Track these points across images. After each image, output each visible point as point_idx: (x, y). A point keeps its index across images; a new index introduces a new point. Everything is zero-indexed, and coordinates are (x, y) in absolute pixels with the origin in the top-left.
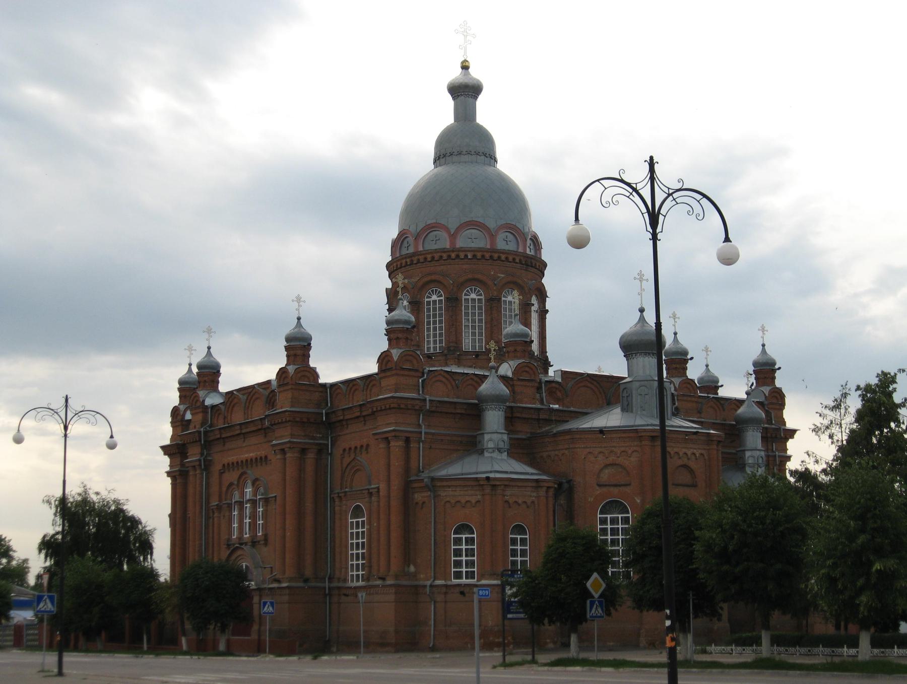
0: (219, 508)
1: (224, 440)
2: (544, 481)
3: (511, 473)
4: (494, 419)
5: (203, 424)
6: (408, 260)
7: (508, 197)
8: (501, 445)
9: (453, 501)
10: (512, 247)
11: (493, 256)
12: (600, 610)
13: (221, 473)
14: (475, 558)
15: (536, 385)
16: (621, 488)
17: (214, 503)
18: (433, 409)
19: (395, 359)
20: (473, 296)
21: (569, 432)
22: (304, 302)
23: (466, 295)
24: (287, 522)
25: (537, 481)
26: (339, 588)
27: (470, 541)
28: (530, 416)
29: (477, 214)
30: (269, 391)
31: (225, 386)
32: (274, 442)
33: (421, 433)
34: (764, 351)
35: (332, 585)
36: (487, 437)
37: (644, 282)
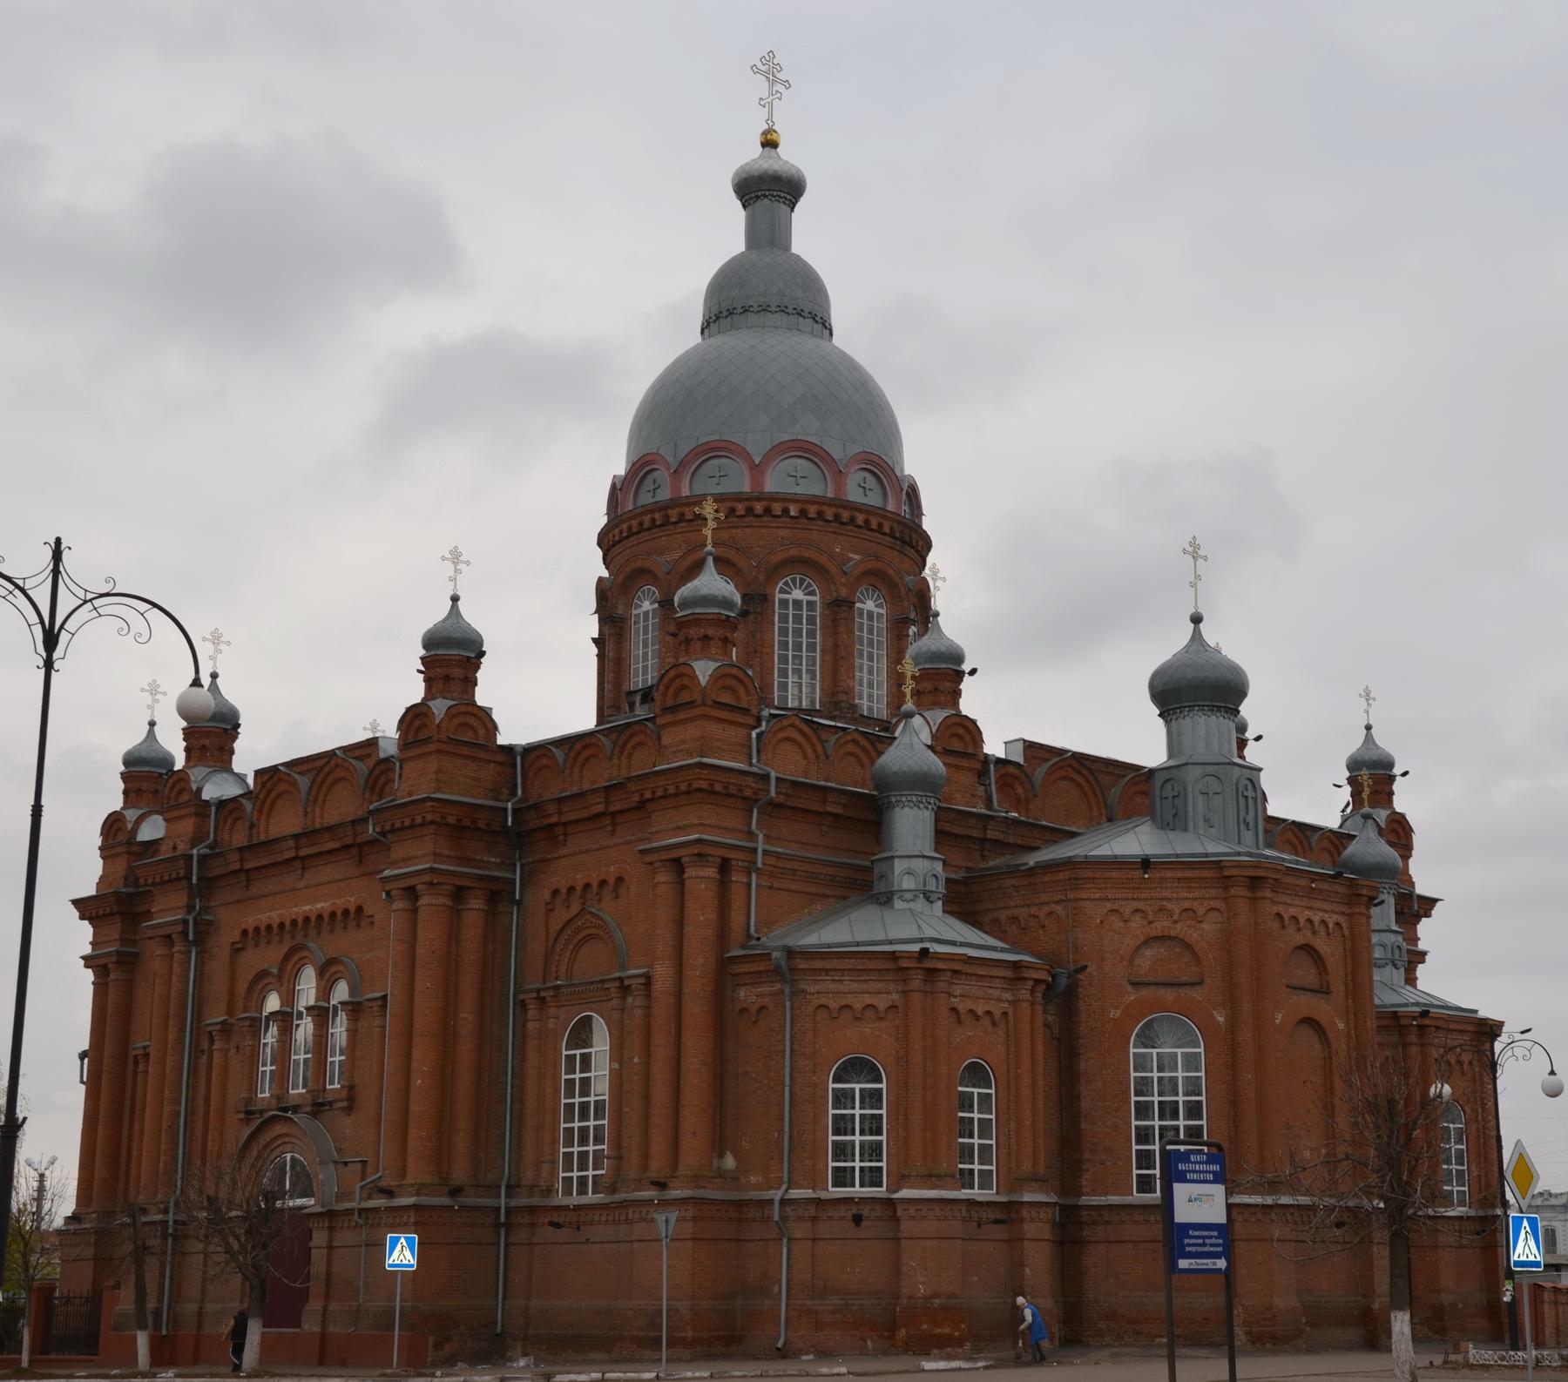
0: (226, 1029)
1: (248, 875)
2: (1029, 966)
3: (963, 944)
4: (912, 826)
5: (195, 841)
6: (657, 515)
7: (860, 407)
8: (932, 885)
9: (834, 1005)
10: (874, 499)
11: (836, 515)
12: (1532, 1243)
13: (236, 951)
14: (884, 1138)
15: (978, 766)
16: (1182, 991)
17: (215, 1018)
18: (781, 799)
19: (703, 681)
20: (797, 594)
21: (1069, 863)
22: (468, 563)
23: (782, 591)
24: (417, 1054)
25: (1016, 966)
26: (532, 1210)
27: (873, 1098)
28: (967, 832)
29: (807, 429)
30: (371, 762)
31: (253, 752)
32: (387, 873)
33: (755, 850)
34: (1369, 738)
35: (513, 1203)
36: (899, 866)
37: (1200, 561)
